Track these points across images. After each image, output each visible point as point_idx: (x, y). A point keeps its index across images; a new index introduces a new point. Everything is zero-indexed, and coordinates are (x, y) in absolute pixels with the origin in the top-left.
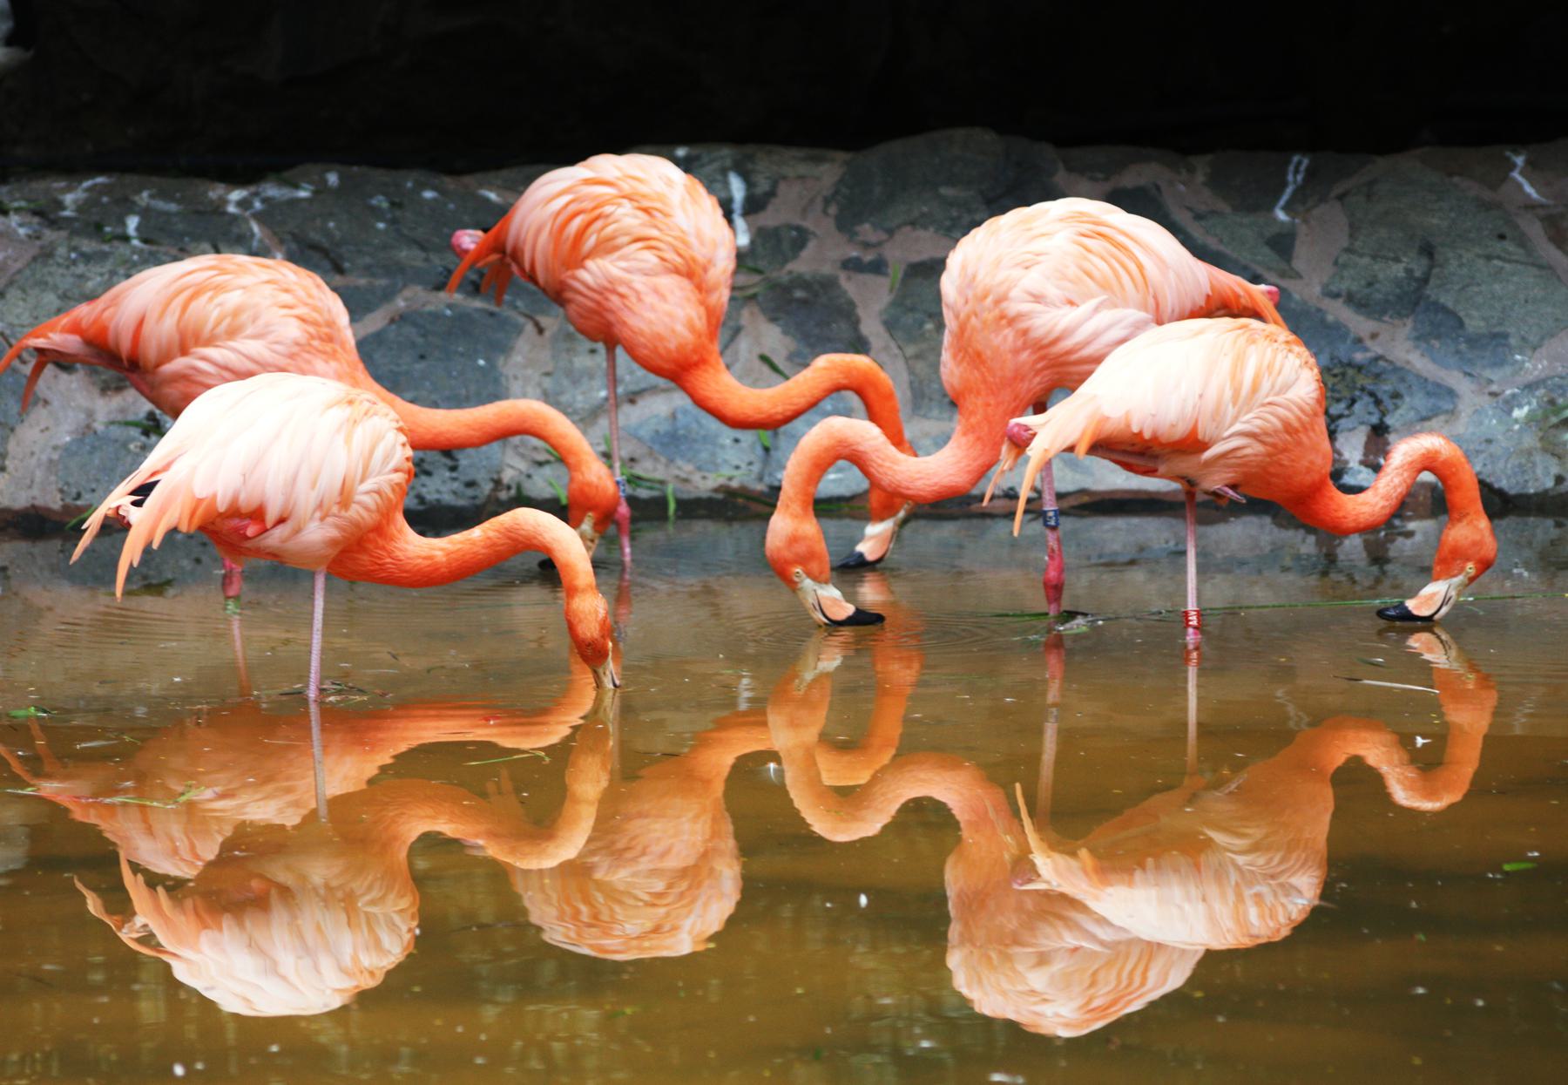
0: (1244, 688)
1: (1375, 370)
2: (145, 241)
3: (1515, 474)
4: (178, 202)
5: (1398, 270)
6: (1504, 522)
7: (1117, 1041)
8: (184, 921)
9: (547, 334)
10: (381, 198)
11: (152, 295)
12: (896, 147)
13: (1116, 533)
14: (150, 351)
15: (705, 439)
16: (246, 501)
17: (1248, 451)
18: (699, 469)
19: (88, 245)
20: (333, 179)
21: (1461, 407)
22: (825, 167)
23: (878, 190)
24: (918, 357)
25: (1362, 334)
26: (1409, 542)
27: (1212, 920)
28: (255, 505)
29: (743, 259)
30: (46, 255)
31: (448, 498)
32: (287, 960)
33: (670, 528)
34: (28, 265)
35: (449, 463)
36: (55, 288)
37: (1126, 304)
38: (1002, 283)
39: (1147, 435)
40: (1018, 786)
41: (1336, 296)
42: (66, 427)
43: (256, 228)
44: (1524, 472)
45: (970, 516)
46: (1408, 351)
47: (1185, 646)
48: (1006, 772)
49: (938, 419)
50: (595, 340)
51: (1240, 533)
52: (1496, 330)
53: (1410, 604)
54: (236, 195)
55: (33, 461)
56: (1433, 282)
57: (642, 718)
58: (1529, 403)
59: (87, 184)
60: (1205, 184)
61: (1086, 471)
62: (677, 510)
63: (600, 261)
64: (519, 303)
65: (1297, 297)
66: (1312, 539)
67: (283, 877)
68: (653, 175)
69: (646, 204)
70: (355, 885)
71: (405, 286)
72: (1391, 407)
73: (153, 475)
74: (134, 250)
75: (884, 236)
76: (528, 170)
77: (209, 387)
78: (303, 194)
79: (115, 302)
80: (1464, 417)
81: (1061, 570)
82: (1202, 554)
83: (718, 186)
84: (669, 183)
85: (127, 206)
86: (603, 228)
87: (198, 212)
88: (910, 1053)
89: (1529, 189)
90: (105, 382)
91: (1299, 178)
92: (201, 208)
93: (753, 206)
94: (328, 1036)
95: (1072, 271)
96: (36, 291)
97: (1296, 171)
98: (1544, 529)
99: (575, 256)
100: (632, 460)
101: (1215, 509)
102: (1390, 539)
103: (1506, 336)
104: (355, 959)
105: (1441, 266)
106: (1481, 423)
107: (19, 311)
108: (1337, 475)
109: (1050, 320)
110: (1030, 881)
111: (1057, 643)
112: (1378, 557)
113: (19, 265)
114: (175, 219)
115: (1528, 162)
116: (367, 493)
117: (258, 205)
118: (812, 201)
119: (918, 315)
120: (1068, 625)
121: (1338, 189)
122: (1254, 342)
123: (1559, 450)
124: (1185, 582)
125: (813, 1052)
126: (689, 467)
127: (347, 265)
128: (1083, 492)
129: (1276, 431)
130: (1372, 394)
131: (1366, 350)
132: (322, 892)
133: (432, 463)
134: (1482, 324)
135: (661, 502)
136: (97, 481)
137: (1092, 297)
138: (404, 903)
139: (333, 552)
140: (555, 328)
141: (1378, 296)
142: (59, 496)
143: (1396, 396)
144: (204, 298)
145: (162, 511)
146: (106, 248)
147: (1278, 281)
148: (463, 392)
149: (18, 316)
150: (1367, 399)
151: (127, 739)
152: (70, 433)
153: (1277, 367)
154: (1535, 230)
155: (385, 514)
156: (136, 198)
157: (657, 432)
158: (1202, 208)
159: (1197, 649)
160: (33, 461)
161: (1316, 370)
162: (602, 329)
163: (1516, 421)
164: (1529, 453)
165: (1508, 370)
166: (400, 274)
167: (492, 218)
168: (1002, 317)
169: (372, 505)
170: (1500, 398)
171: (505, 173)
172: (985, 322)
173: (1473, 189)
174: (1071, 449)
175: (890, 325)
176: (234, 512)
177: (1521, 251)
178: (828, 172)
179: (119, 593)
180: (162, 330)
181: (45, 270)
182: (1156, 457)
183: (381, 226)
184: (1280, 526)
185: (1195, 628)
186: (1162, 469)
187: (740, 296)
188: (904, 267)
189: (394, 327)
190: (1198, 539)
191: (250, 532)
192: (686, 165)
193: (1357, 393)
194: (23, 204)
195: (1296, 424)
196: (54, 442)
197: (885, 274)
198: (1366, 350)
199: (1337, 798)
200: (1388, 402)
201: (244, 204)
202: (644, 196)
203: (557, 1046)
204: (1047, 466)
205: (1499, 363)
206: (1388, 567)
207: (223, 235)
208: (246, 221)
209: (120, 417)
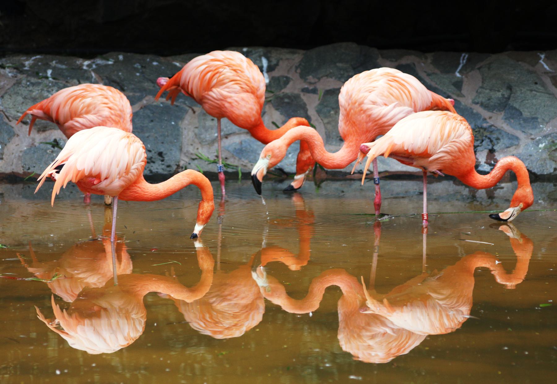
0: (444, 242)
1: (490, 130)
2: (54, 79)
3: (540, 167)
4: (66, 65)
5: (499, 95)
6: (536, 184)
7: (395, 364)
8: (72, 321)
9: (197, 113)
10: (138, 64)
11: (64, 97)
12: (322, 48)
13: (398, 186)
14: (61, 119)
15: (252, 151)
16: (95, 172)
17: (446, 158)
18: (250, 162)
19: (33, 80)
20: (121, 57)
21: (521, 143)
22: (296, 56)
23: (315, 64)
24: (328, 123)
25: (486, 117)
26: (502, 190)
27: (432, 325)
28: (97, 173)
29: (268, 86)
30: (18, 83)
31: (160, 171)
32: (106, 334)
33: (239, 183)
34: (12, 86)
35: (161, 158)
36: (22, 95)
37: (404, 105)
38: (361, 98)
39: (410, 151)
40: (362, 277)
41: (477, 103)
42: (25, 144)
43: (93, 74)
44: (543, 167)
45: (346, 180)
46: (502, 123)
47: (422, 226)
48: (358, 272)
49: (335, 145)
50: (214, 117)
51: (443, 187)
52: (534, 116)
53: (500, 214)
54: (86, 63)
55: (13, 156)
56: (511, 99)
57: (229, 251)
58: (545, 142)
59: (33, 58)
60: (431, 63)
61: (387, 164)
62: (242, 176)
63: (219, 90)
64: (187, 102)
65: (463, 104)
66: (467, 189)
67: (104, 304)
68: (235, 57)
69: (235, 68)
70: (129, 307)
71: (146, 96)
72: (496, 143)
73: (62, 162)
74: (50, 82)
75: (317, 80)
76: (190, 55)
77: (78, 131)
78: (110, 63)
79: (53, 100)
80: (522, 147)
81: (380, 199)
82: (429, 194)
83: (258, 62)
84: (242, 61)
85: (48, 66)
86: (219, 77)
87: (73, 69)
88: (322, 368)
89: (546, 66)
90: (39, 128)
91: (465, 61)
92: (74, 67)
93: (270, 69)
94: (115, 362)
95: (386, 93)
96: (14, 96)
97: (463, 59)
98: (550, 187)
99: (209, 87)
100: (226, 158)
101: (433, 178)
102: (495, 189)
103: (537, 118)
104: (129, 334)
105: (514, 93)
106: (528, 149)
107: (9, 103)
108: (477, 167)
109: (378, 111)
110: (366, 310)
111: (378, 225)
112: (491, 196)
113: (9, 87)
114: (65, 71)
115: (546, 57)
116: (134, 169)
117: (94, 66)
118: (291, 68)
119: (329, 109)
120: (382, 219)
121: (478, 66)
122: (449, 119)
123: (555, 159)
124: (423, 204)
125: (289, 369)
126: (246, 161)
127: (126, 88)
128: (386, 172)
129: (456, 151)
130: (489, 138)
131: (487, 123)
132: (118, 310)
133: (155, 159)
134: (529, 114)
135: (236, 173)
136: (36, 163)
137: (393, 102)
138: (140, 315)
139: (121, 190)
140: (199, 112)
141: (492, 104)
142: (22, 169)
143: (498, 139)
144: (78, 100)
145: (66, 175)
146: (40, 81)
147: (455, 97)
148: (166, 133)
149: (8, 105)
150: (487, 140)
151: (55, 255)
152: (25, 146)
153: (457, 128)
154: (548, 81)
155: (138, 176)
156: (51, 63)
157: (235, 149)
158: (430, 72)
159: (426, 228)
160: (13, 156)
161: (471, 130)
162: (220, 112)
163: (540, 149)
164: (545, 160)
165: (537, 130)
166: (145, 92)
167: (173, 72)
168: (361, 110)
169: (135, 174)
170: (535, 140)
171: (182, 56)
172: (355, 112)
173: (526, 66)
174: (383, 155)
175: (319, 112)
176: (90, 175)
177: (542, 88)
178: (297, 57)
179: (52, 204)
180: (65, 111)
181: (18, 89)
182: (413, 159)
183: (138, 74)
184: (456, 184)
185: (426, 220)
186: (415, 163)
187: (268, 102)
188: (324, 91)
189: (142, 110)
190: (427, 189)
191: (95, 182)
192: (247, 55)
193: (484, 138)
194: (10, 65)
195: (463, 149)
196: (21, 150)
197: (317, 94)
198: (487, 123)
199: (475, 281)
200: (495, 141)
201: (89, 66)
202: (234, 65)
203: (197, 366)
204: (374, 161)
205: (535, 128)
206: (494, 200)
207: (82, 77)
208: (90, 72)
209: (44, 141)
